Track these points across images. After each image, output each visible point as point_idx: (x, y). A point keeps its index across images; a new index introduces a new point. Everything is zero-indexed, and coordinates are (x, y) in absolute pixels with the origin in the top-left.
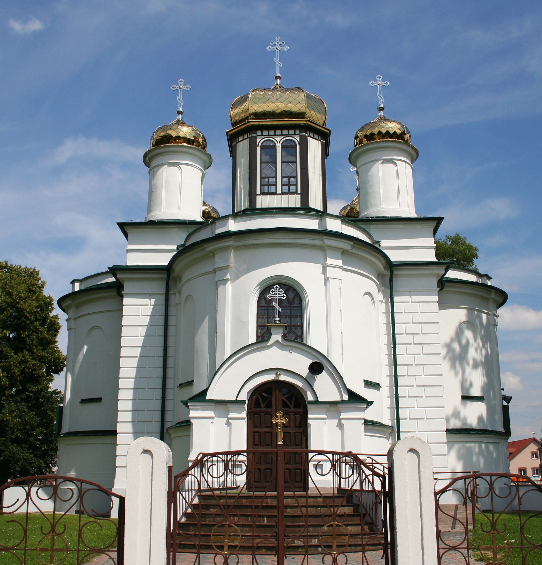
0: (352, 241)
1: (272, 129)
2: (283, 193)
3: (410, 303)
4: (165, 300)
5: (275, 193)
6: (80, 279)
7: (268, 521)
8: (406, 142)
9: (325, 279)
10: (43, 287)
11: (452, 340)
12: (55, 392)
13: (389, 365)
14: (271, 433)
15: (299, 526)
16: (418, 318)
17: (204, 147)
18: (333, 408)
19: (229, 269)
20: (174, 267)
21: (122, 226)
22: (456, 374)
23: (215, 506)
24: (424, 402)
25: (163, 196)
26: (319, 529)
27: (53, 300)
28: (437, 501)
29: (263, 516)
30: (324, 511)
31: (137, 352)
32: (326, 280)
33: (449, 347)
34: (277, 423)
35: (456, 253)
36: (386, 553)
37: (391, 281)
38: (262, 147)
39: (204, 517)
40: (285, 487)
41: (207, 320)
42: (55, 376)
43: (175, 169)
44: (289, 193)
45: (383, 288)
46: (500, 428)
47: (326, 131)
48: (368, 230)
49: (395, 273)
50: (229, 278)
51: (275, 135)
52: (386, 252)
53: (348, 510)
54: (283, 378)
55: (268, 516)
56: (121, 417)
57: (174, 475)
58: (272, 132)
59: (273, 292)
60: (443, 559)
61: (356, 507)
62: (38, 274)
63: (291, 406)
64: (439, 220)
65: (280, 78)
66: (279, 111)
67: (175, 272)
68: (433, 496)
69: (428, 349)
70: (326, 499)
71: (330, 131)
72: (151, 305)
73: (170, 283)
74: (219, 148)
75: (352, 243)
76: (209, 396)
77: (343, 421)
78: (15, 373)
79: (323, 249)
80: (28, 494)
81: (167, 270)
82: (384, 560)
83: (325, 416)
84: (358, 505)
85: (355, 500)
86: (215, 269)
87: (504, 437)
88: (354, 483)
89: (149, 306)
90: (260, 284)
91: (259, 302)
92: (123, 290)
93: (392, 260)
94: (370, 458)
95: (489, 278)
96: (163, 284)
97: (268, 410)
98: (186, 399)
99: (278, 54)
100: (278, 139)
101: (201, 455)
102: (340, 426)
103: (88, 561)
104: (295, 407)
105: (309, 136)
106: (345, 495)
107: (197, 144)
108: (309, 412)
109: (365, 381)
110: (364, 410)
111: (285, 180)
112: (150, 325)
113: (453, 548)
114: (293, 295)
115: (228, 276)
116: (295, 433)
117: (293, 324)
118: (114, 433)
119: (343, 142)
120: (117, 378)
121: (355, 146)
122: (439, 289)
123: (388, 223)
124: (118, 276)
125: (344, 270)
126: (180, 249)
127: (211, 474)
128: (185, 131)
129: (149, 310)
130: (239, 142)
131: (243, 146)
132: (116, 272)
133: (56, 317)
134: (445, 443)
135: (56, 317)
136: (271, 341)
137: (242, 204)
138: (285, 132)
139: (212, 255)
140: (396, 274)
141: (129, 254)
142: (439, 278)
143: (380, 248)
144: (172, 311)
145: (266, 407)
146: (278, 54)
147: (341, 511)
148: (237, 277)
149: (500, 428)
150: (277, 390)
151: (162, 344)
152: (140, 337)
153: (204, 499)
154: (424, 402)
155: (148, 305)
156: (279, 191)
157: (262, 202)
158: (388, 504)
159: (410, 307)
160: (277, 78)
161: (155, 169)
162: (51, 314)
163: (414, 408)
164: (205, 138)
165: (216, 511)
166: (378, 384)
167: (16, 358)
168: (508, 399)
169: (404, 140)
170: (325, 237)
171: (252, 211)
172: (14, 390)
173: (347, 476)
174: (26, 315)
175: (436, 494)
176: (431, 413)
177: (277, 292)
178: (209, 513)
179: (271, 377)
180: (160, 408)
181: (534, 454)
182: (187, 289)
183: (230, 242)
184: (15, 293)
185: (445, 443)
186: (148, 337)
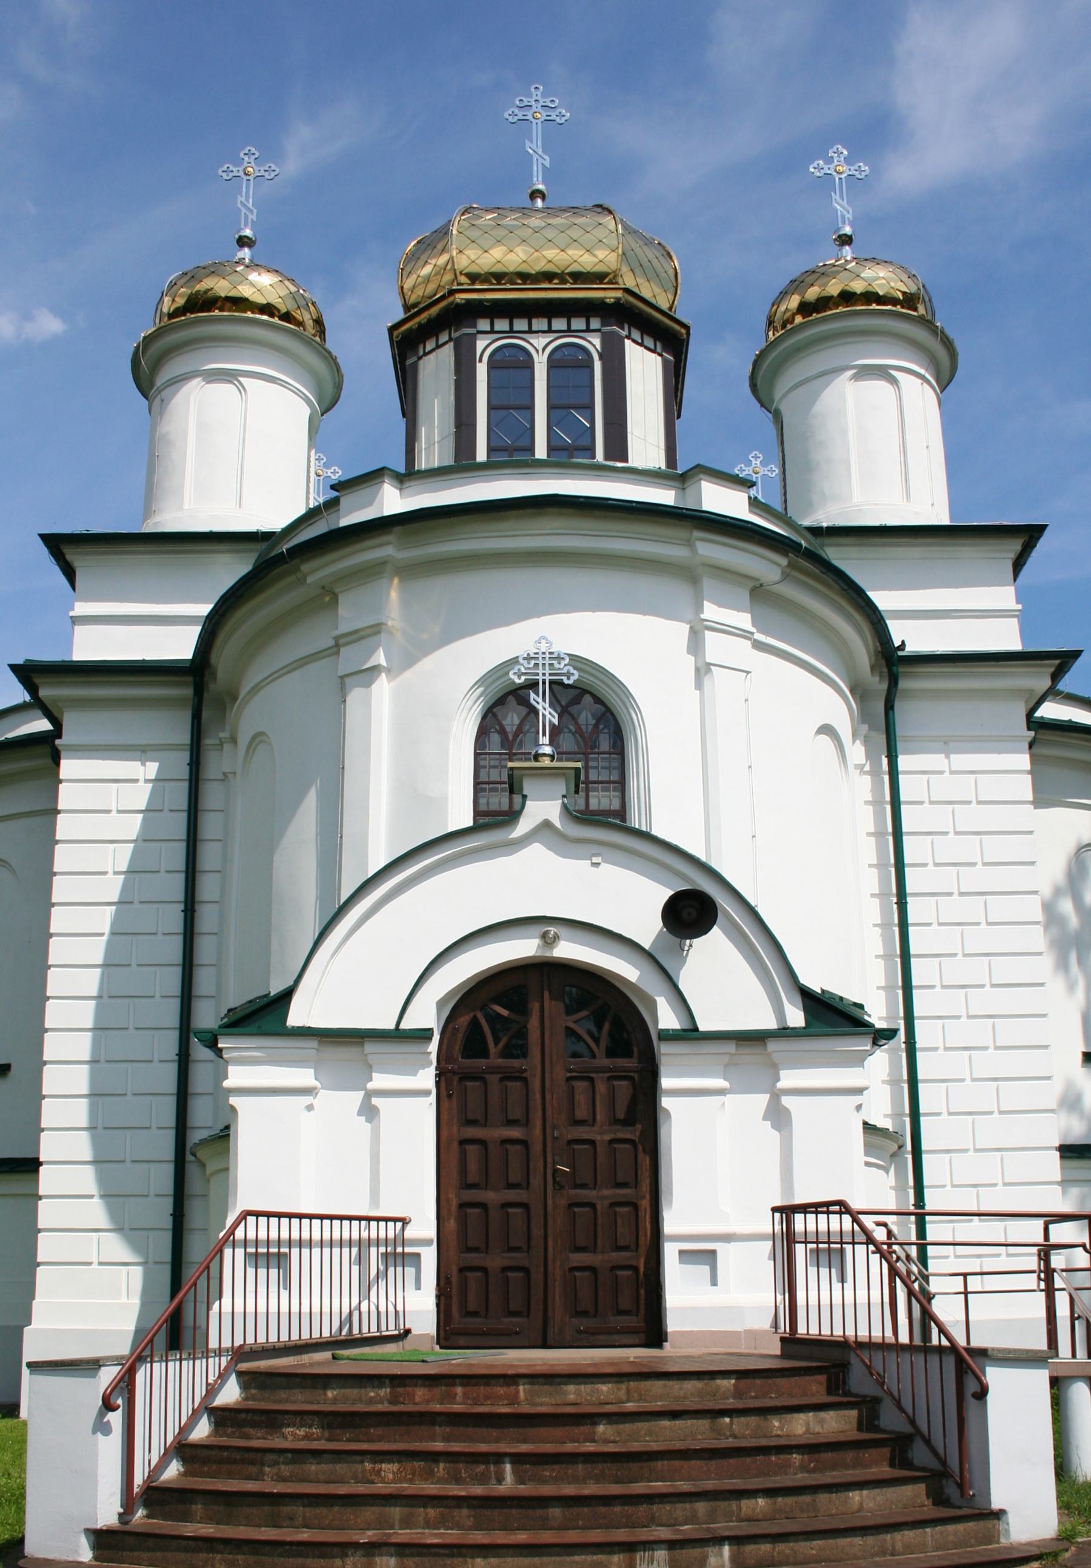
0: (785, 554)
1: (521, 315)
3: (947, 774)
7: (520, 1479)
8: (927, 323)
9: (697, 670)
11: (1058, 892)
13: (887, 957)
14: (524, 1143)
16: (972, 817)
18: (749, 1054)
19: (383, 635)
20: (213, 658)
21: (58, 545)
22: (1071, 987)
23: (301, 1417)
24: (990, 1063)
25: (189, 459)
26: (734, 1504)
29: (498, 1458)
30: (740, 1431)
31: (103, 920)
32: (703, 670)
33: (1049, 908)
37: (889, 707)
38: (492, 366)
39: (253, 1462)
40: (579, 1332)
41: (311, 801)
43: (225, 391)
45: (865, 728)
47: (677, 327)
49: (903, 684)
50: (383, 662)
51: (530, 331)
53: (835, 1424)
54: (569, 950)
55: (518, 1459)
56: (51, 1113)
58: (521, 324)
61: (868, 1409)
63: (600, 1051)
64: (1031, 534)
65: (543, 197)
67: (220, 674)
69: (1000, 909)
70: (744, 1383)
72: (147, 781)
73: (206, 714)
74: (365, 352)
75: (784, 562)
77: (786, 1101)
79: (690, 575)
81: (197, 672)
83: (720, 1083)
84: (876, 1401)
85: (859, 1382)
89: (141, 783)
90: (485, 680)
91: (482, 733)
94: (885, 1225)
96: (184, 719)
97: (516, 1063)
99: (537, 130)
100: (539, 341)
102: (778, 1116)
104: (610, 1053)
105: (628, 337)
106: (819, 1363)
107: (298, 330)
108: (663, 1070)
110: (858, 1060)
112: (144, 840)
115: (380, 658)
116: (612, 1142)
118: (31, 1166)
119: (721, 360)
120: (39, 998)
123: (877, 540)
125: (758, 646)
128: (261, 285)
129: (140, 796)
130: (426, 354)
131: (436, 366)
134: (1058, 1183)
136: (524, 826)
138: (559, 324)
139: (327, 598)
140: (903, 690)
141: (78, 629)
144: (212, 796)
145: (507, 1053)
146: (537, 130)
147: (800, 1426)
148: (409, 660)
150: (546, 994)
151: (179, 894)
152: (110, 875)
153: (262, 1387)
154: (990, 1063)
155: (136, 781)
159: (946, 787)
161: (164, 394)
163: (962, 1080)
165: (307, 1437)
170: (697, 534)
176: (1015, 1095)
178: (277, 1442)
179: (522, 948)
180: (172, 1086)
182: (251, 717)
183: (386, 549)
185: (1058, 1183)
186: (137, 876)
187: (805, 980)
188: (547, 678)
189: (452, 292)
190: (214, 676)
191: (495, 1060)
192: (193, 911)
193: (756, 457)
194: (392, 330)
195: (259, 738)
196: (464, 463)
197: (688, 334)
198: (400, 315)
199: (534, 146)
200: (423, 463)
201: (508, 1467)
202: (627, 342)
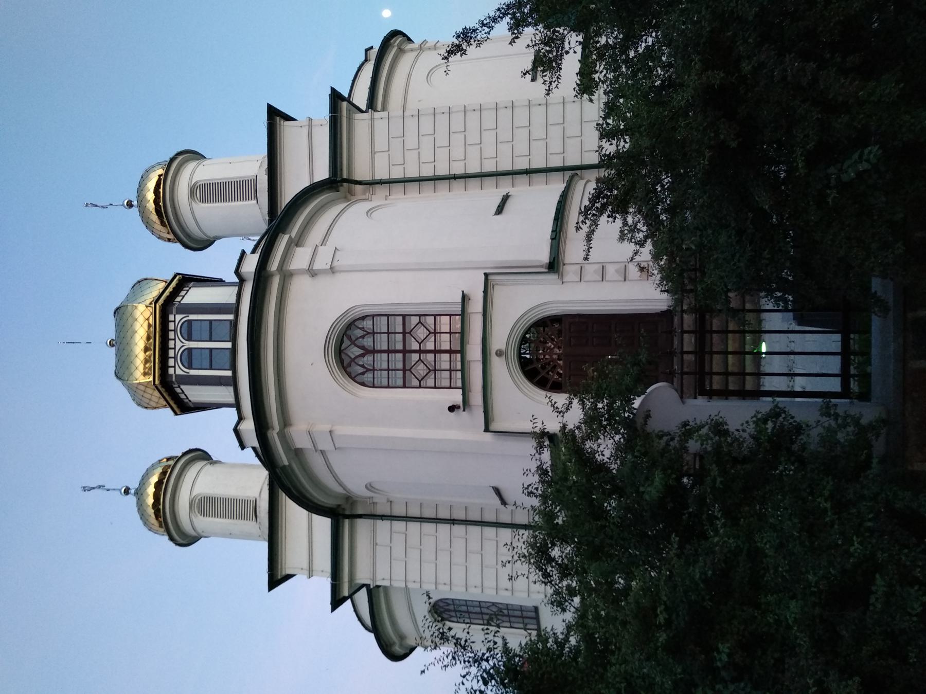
21: (274, 581)
38: (190, 368)
51: (175, 349)
67: (339, 503)
93: (327, 177)
100: (179, 344)
109: (496, 214)
131: (194, 394)
182: (357, 487)
189: (156, 387)
192: (454, 520)
194: (176, 414)
196: (233, 382)
197: (179, 274)
198: (169, 410)
200: (232, 400)
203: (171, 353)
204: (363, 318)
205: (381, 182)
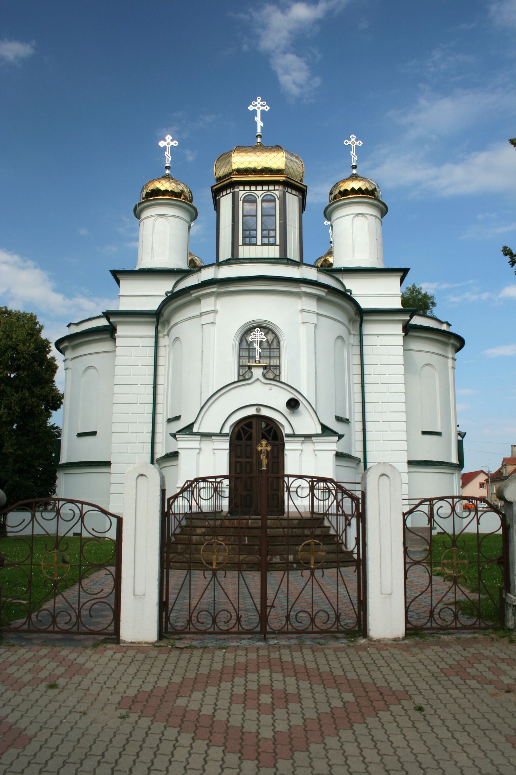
2: (263, 244)
4: (155, 342)
5: (256, 245)
6: (76, 323)
10: (41, 331)
12: (52, 427)
15: (276, 545)
17: (191, 201)
20: (162, 311)
27: (50, 343)
28: (404, 521)
34: (261, 450)
35: (415, 304)
36: (358, 568)
38: (244, 201)
42: (54, 413)
44: (269, 244)
46: (454, 460)
48: (341, 280)
52: (358, 299)
54: (265, 412)
57: (167, 496)
59: (254, 334)
60: (408, 573)
62: (35, 319)
64: (405, 272)
66: (259, 168)
68: (402, 517)
71: (306, 187)
74: (203, 199)
75: (326, 291)
76: (195, 430)
78: (15, 410)
80: (33, 516)
82: (356, 574)
86: (201, 313)
87: (458, 469)
88: (329, 507)
92: (116, 332)
95: (449, 325)
98: (174, 432)
100: (259, 193)
101: (189, 483)
103: (87, 577)
105: (287, 192)
109: (336, 417)
111: (265, 232)
113: (418, 563)
114: (272, 338)
117: (272, 364)
121: (330, 201)
122: (404, 334)
124: (111, 320)
126: (169, 295)
127: (202, 497)
130: (223, 196)
131: (226, 201)
132: (109, 316)
133: (53, 359)
135: (53, 359)
137: (225, 253)
142: (405, 324)
143: (352, 296)
145: (246, 440)
149: (454, 460)
156: (259, 243)
157: (244, 252)
158: (361, 524)
160: (257, 136)
162: (49, 356)
164: (191, 192)
166: (348, 420)
167: (16, 397)
168: (462, 435)
169: (375, 196)
171: (235, 259)
172: (15, 425)
173: (325, 499)
174: (25, 357)
175: (404, 514)
177: (258, 334)
179: (252, 411)
181: (481, 485)
184: (14, 336)
187: (321, 421)
188: (259, 340)
190: (162, 316)
191: (244, 441)
193: (353, 137)
195: (177, 339)
199: (258, 119)
201: (246, 538)
202: (287, 193)
203: (253, 188)
204: (279, 342)
205: (361, 341)
